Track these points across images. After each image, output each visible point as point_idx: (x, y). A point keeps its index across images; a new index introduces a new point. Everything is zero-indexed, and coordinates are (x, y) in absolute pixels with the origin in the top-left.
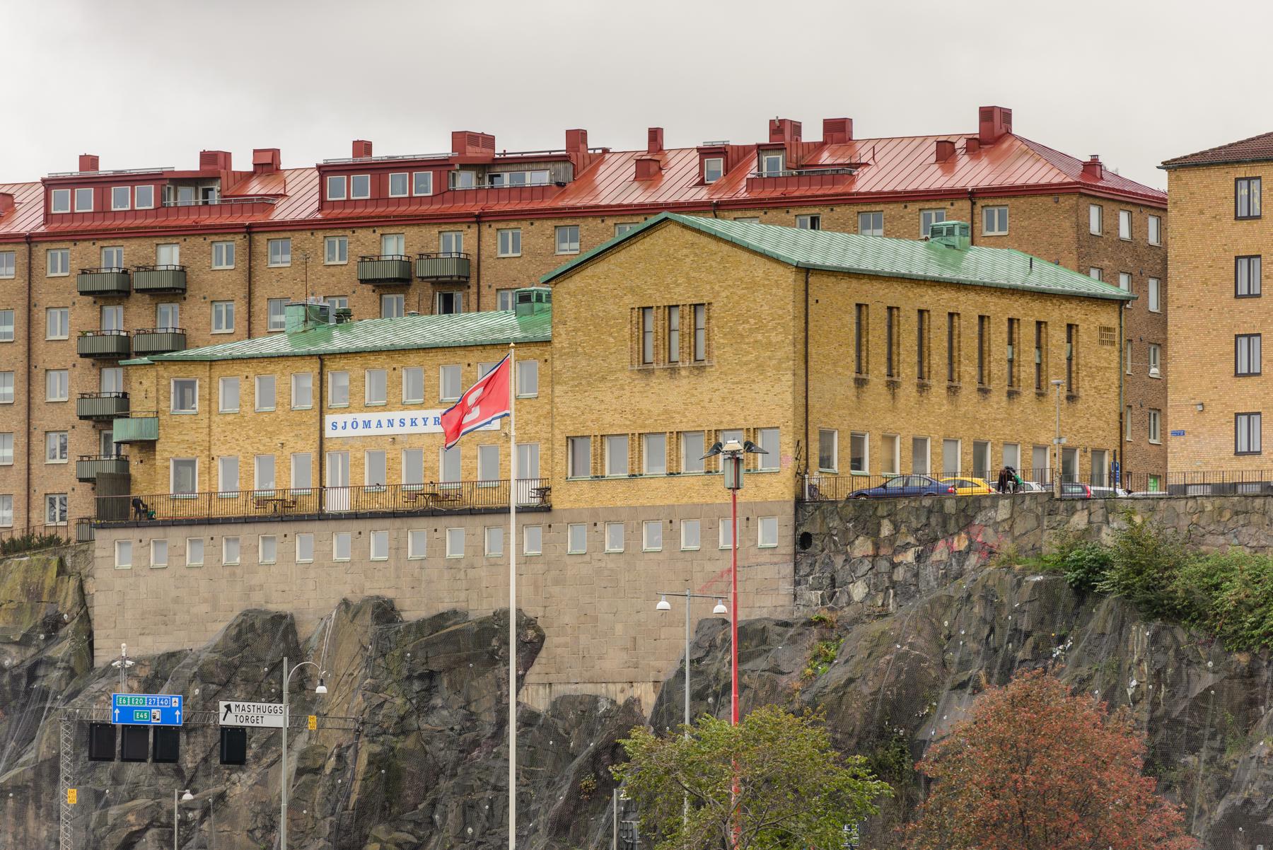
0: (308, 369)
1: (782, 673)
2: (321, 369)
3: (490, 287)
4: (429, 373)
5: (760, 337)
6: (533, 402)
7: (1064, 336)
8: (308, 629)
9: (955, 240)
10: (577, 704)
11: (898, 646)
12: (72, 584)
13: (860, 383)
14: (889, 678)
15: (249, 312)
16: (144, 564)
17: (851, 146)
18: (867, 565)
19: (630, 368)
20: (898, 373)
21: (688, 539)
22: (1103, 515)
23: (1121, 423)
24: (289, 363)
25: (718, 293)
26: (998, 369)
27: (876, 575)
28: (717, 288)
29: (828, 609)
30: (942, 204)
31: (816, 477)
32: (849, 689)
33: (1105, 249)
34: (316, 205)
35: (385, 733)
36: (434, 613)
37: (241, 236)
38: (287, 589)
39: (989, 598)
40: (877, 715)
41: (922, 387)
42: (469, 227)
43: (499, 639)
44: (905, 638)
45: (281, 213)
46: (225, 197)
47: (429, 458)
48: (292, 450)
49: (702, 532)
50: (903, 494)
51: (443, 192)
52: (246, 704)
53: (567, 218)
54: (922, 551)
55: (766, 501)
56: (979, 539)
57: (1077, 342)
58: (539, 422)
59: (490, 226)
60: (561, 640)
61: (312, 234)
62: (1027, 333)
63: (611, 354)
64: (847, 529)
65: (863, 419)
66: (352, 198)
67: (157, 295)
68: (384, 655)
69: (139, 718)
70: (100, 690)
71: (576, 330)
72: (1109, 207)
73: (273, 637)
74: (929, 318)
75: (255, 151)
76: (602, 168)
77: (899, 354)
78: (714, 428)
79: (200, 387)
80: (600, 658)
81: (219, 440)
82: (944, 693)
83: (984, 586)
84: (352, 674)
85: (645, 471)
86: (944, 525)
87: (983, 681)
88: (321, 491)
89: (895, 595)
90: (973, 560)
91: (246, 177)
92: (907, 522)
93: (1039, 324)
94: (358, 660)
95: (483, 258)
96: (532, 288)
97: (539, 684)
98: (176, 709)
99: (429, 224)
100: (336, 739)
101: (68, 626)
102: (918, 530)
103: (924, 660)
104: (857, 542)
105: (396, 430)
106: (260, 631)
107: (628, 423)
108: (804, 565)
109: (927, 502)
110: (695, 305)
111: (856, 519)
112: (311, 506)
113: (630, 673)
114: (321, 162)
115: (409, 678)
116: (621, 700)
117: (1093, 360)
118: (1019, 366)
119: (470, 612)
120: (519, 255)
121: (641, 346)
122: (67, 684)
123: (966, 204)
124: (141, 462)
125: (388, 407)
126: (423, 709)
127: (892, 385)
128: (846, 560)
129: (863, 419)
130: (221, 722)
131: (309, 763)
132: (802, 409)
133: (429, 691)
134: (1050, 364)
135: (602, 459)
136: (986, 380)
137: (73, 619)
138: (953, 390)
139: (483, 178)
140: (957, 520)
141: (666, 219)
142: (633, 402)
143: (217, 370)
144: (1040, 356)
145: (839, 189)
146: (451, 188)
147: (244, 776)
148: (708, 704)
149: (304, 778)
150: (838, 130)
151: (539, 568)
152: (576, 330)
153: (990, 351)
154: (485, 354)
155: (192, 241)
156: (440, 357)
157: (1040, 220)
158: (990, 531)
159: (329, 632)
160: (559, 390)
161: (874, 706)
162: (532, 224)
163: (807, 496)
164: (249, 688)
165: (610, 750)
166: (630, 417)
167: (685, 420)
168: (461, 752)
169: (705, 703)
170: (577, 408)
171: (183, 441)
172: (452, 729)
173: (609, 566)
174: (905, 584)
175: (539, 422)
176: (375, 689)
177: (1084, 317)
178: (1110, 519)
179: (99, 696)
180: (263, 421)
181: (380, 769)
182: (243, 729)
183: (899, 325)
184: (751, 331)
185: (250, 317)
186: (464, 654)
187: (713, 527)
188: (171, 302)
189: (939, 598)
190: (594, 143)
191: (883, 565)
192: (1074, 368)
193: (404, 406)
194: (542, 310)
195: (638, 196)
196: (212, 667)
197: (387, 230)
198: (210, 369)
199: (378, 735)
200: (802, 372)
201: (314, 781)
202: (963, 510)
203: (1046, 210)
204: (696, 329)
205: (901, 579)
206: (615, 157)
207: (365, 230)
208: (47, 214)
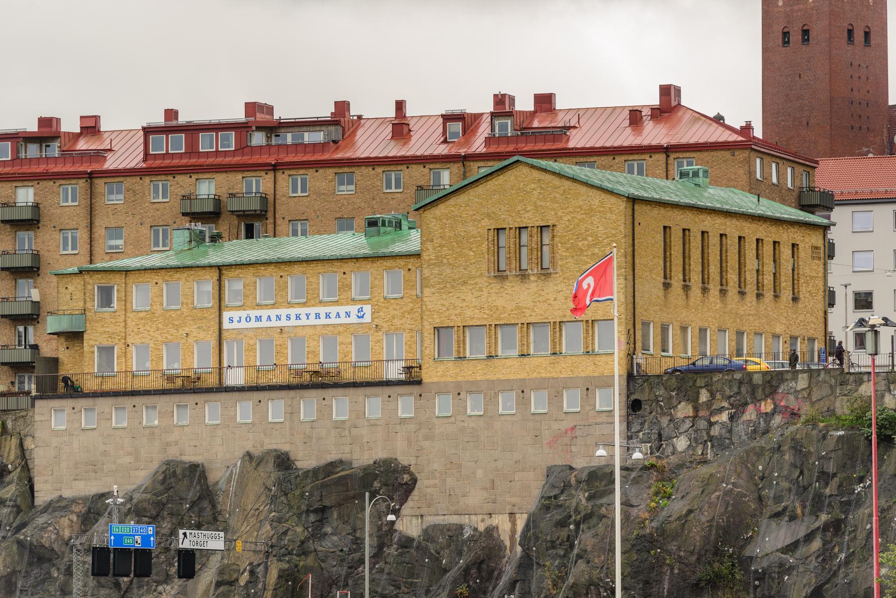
0: (208, 277)
1: (632, 506)
2: (220, 277)
3: (283, 218)
4: (311, 279)
5: (596, 251)
6: (398, 301)
7: (790, 252)
8: (217, 475)
9: (700, 180)
10: (445, 530)
11: (724, 485)
12: (14, 441)
13: (667, 286)
14: (720, 509)
15: (91, 237)
16: (76, 426)
17: (556, 114)
18: (688, 424)
19: (487, 275)
20: (689, 279)
21: (538, 404)
22: (885, 385)
23: (825, 318)
24: (192, 272)
25: (561, 217)
26: (751, 277)
27: (696, 431)
28: (560, 213)
29: (657, 457)
30: (643, 157)
31: (639, 359)
32: (690, 518)
33: (765, 191)
34: (141, 156)
35: (289, 554)
36: (323, 462)
37: (84, 181)
38: (198, 444)
39: (797, 447)
40: (713, 538)
41: (705, 290)
42: (266, 174)
43: (381, 481)
44: (729, 479)
45: (111, 163)
46: (63, 151)
47: (311, 344)
48: (195, 339)
49: (549, 399)
50: (719, 370)
51: (243, 147)
52: (197, 532)
53: (345, 166)
54: (734, 413)
55: (603, 376)
56: (782, 404)
57: (798, 257)
58: (404, 317)
59: (283, 173)
60: (432, 482)
61: (141, 179)
62: (768, 249)
63: (471, 264)
64: (671, 397)
65: (668, 314)
66: (170, 152)
67: (16, 225)
68: (286, 495)
69: (128, 543)
70: (46, 523)
71: (441, 246)
72: (767, 159)
73: (192, 482)
74: (708, 238)
75: (81, 117)
76: (360, 132)
77: (690, 265)
78: (558, 320)
79: (118, 291)
80: (464, 496)
81: (133, 331)
82: (764, 522)
83: (793, 439)
84: (258, 509)
85: (500, 353)
86: (753, 393)
87: (799, 511)
88: (220, 369)
89: (712, 446)
90: (778, 420)
91: (76, 137)
92: (722, 391)
93: (775, 243)
94: (263, 498)
95: (278, 197)
96: (379, 216)
97: (412, 516)
98: (151, 536)
99: (235, 171)
100: (247, 558)
101: (13, 474)
102: (731, 397)
103: (745, 496)
104: (679, 406)
105: (284, 323)
106: (180, 477)
107: (486, 316)
108: (635, 424)
109: (738, 376)
110: (542, 227)
111: (679, 389)
112: (212, 381)
113: (489, 507)
114: (145, 125)
115: (308, 512)
116: (481, 528)
117: (808, 271)
118: (763, 274)
119: (353, 462)
120: (307, 194)
121: (496, 258)
122: (15, 519)
123: (662, 157)
124: (68, 348)
125: (277, 305)
126: (317, 534)
127: (686, 288)
128: (670, 420)
129: (668, 314)
130: (181, 546)
131: (226, 577)
132: (631, 306)
133: (321, 522)
134: (782, 274)
135: (464, 344)
136: (742, 284)
137: (16, 468)
138: (723, 292)
139: (271, 137)
140: (764, 390)
141: (518, 161)
142: (490, 300)
143: (131, 278)
144: (775, 267)
145: (559, 145)
146: (249, 144)
147: (168, 588)
148: (570, 530)
149: (221, 589)
150: (545, 102)
151: (412, 427)
152: (441, 246)
153: (745, 263)
154: (358, 265)
155: (43, 184)
156: (320, 267)
157: (720, 168)
158: (791, 397)
159: (235, 477)
160: (427, 291)
161: (710, 531)
162: (317, 171)
163: (635, 372)
164: (174, 520)
165: (476, 566)
166: (487, 312)
167: (534, 314)
168: (349, 568)
169: (566, 529)
170: (443, 305)
171: (105, 332)
172: (342, 551)
173: (471, 426)
174: (721, 438)
175: (404, 317)
176: (280, 520)
177: (802, 238)
178: (892, 388)
179: (47, 527)
180: (171, 316)
181: (287, 581)
182: (192, 550)
183: (690, 243)
184: (590, 247)
185: (91, 241)
186: (351, 493)
187: (558, 395)
188: (27, 230)
189: (754, 448)
190: (354, 111)
191: (703, 424)
192: (796, 277)
193: (290, 305)
194: (385, 233)
195: (394, 150)
196: (145, 505)
197: (201, 176)
198: (126, 277)
199: (284, 555)
200: (630, 278)
201: (230, 591)
202: (769, 382)
203: (725, 161)
204: (542, 245)
205: (717, 434)
206: (369, 123)
207: (183, 176)
208: (147, 156)
